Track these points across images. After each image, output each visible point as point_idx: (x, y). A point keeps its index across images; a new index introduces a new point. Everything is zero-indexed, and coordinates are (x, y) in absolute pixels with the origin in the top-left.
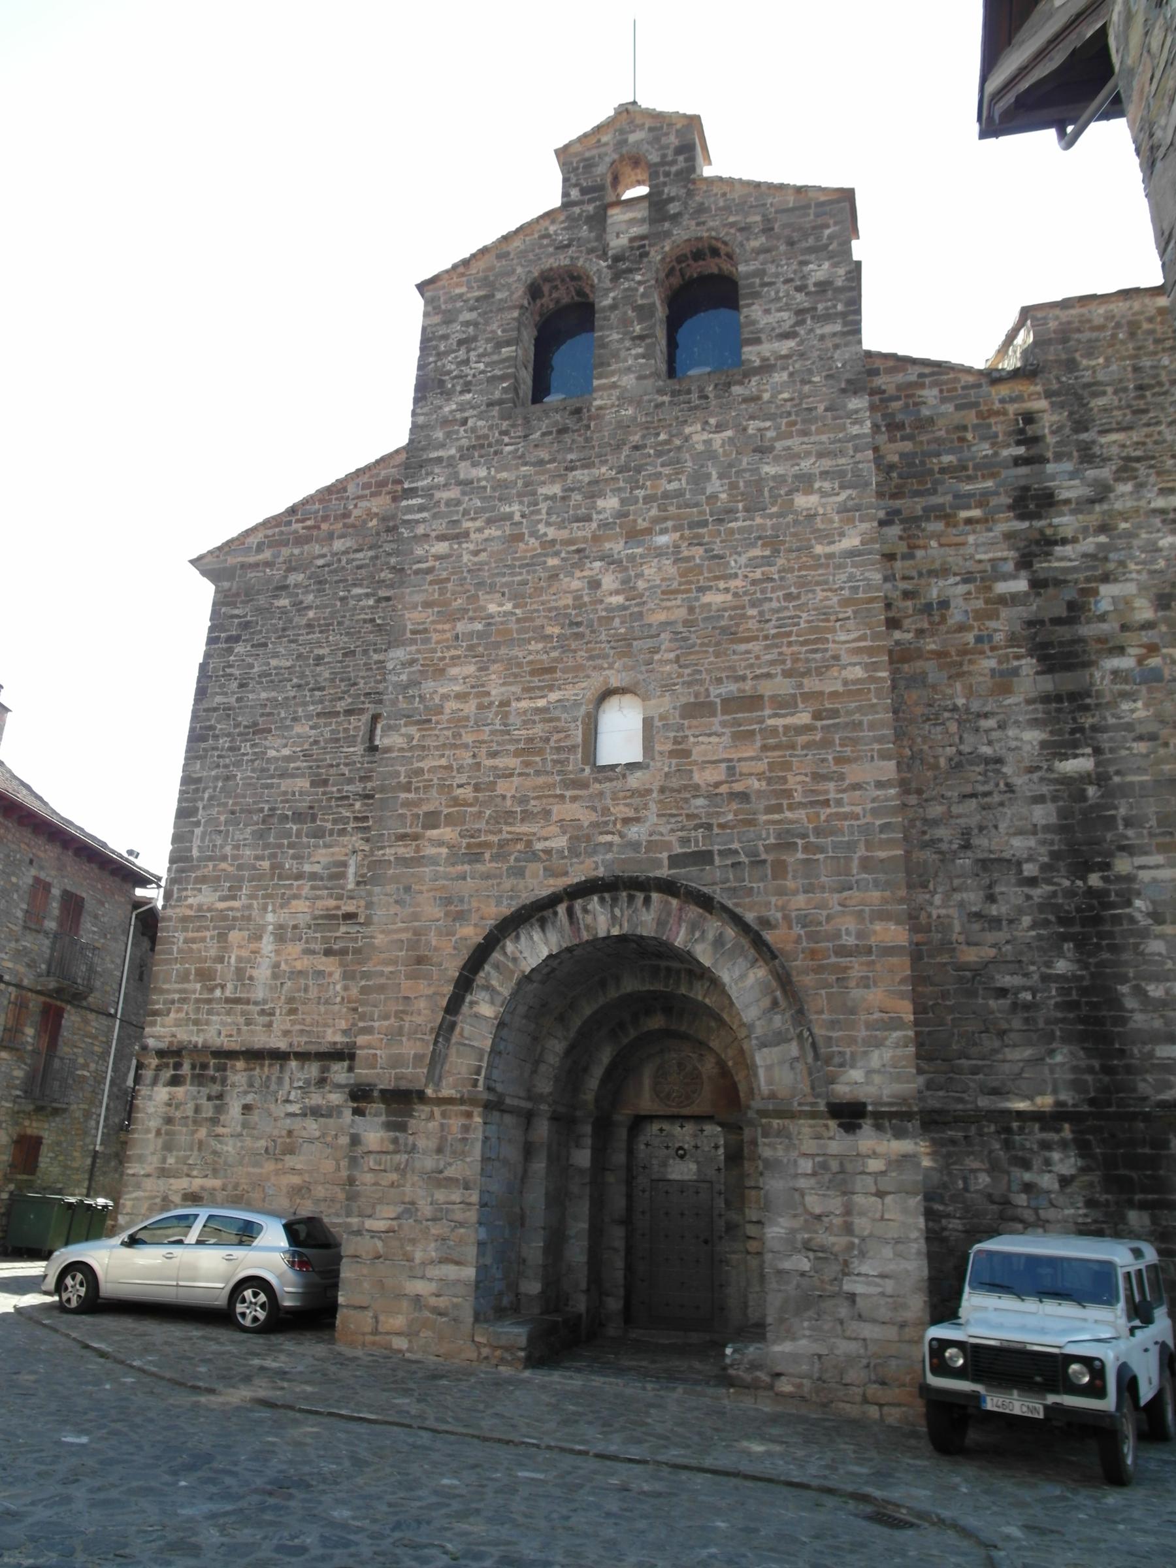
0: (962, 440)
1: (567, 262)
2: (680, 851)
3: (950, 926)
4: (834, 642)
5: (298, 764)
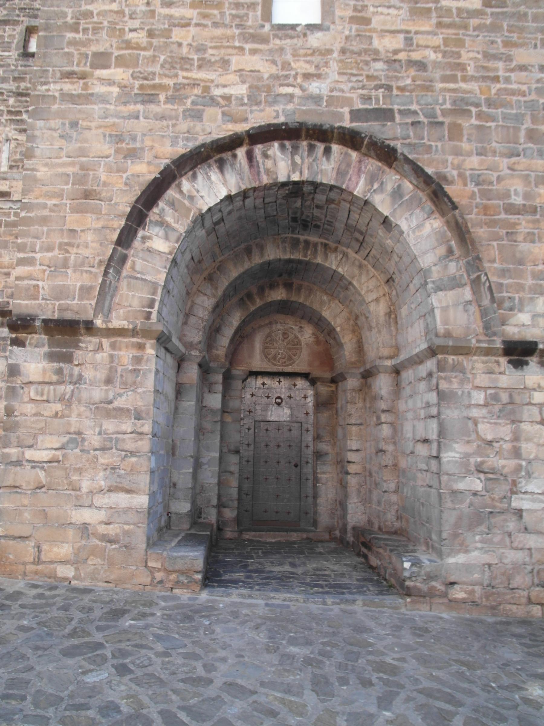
2: (361, 107)
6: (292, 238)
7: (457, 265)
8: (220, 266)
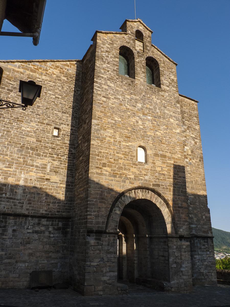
4: (176, 149)
5: (32, 134)
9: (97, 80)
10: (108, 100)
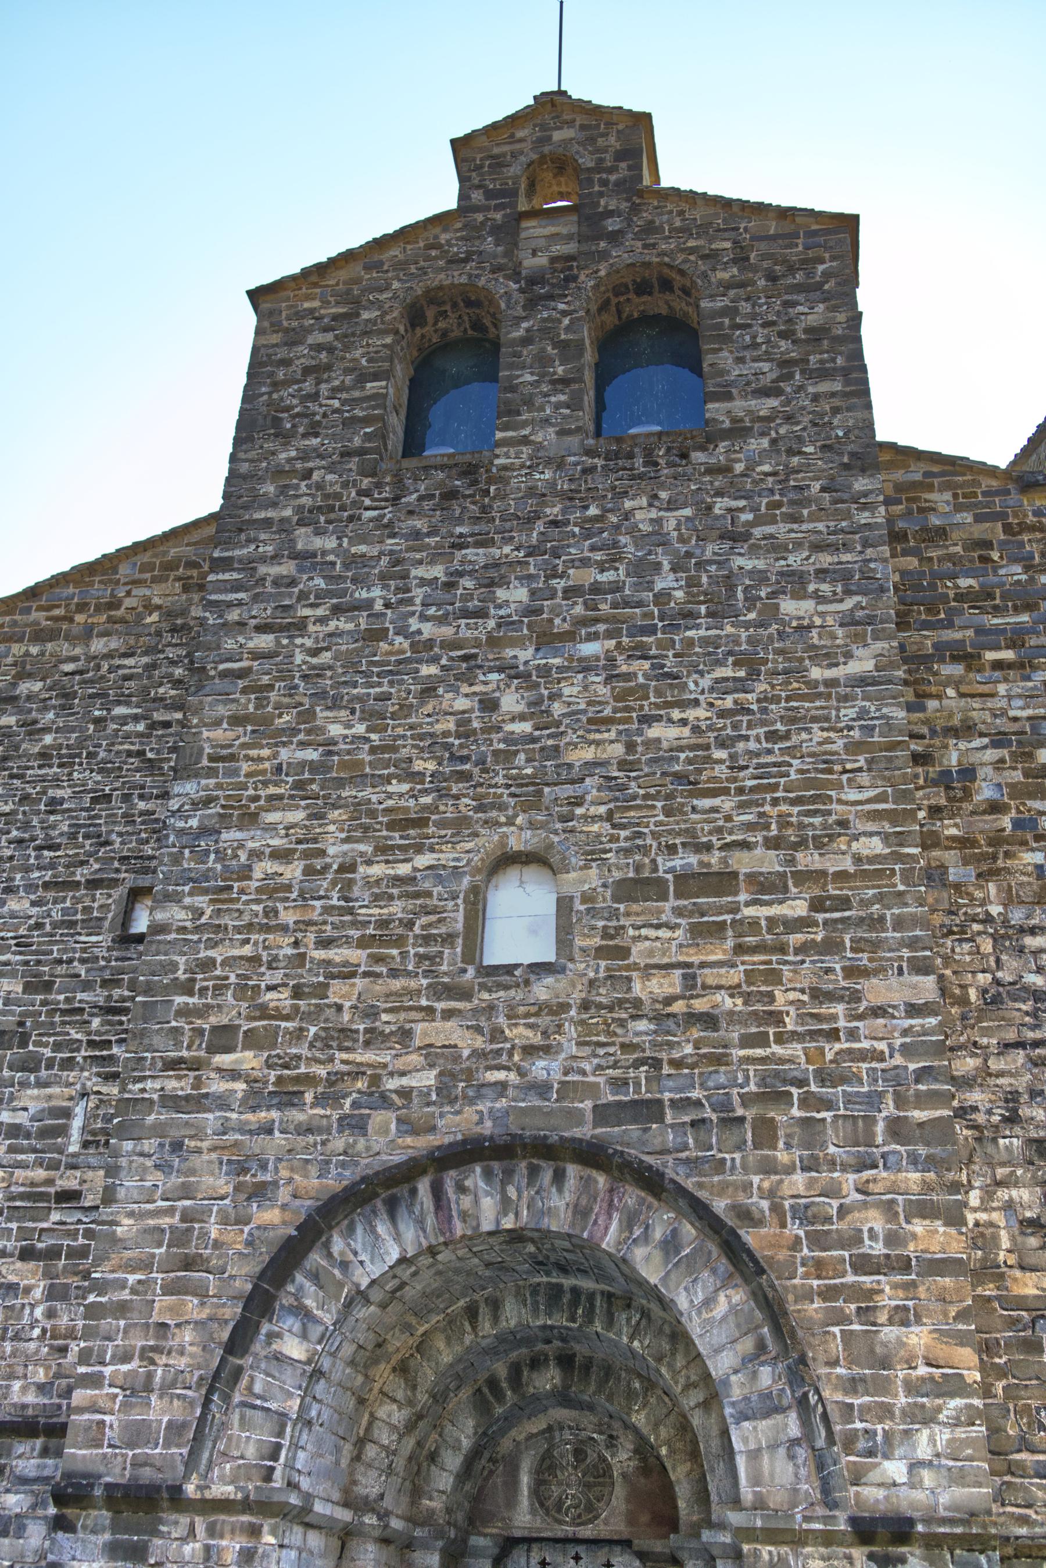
0: (985, 559)
1: (464, 279)
2: (611, 1098)
3: (995, 1239)
4: (840, 801)
6: (549, 1283)
7: (773, 1371)
8: (421, 1343)
9: (227, 550)
10: (285, 642)
